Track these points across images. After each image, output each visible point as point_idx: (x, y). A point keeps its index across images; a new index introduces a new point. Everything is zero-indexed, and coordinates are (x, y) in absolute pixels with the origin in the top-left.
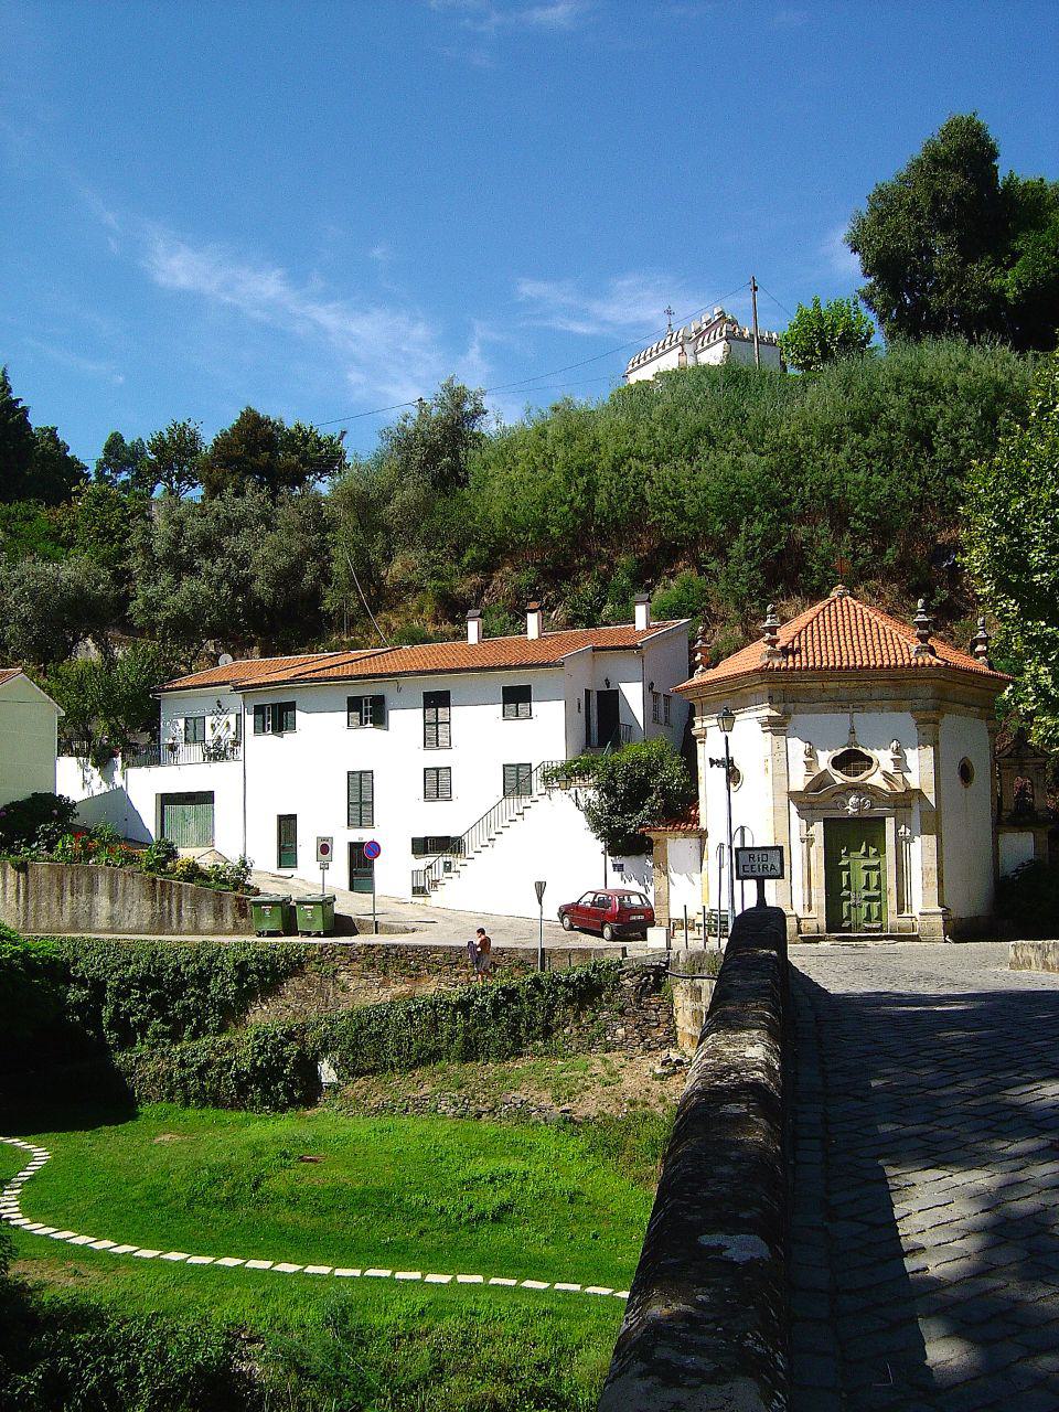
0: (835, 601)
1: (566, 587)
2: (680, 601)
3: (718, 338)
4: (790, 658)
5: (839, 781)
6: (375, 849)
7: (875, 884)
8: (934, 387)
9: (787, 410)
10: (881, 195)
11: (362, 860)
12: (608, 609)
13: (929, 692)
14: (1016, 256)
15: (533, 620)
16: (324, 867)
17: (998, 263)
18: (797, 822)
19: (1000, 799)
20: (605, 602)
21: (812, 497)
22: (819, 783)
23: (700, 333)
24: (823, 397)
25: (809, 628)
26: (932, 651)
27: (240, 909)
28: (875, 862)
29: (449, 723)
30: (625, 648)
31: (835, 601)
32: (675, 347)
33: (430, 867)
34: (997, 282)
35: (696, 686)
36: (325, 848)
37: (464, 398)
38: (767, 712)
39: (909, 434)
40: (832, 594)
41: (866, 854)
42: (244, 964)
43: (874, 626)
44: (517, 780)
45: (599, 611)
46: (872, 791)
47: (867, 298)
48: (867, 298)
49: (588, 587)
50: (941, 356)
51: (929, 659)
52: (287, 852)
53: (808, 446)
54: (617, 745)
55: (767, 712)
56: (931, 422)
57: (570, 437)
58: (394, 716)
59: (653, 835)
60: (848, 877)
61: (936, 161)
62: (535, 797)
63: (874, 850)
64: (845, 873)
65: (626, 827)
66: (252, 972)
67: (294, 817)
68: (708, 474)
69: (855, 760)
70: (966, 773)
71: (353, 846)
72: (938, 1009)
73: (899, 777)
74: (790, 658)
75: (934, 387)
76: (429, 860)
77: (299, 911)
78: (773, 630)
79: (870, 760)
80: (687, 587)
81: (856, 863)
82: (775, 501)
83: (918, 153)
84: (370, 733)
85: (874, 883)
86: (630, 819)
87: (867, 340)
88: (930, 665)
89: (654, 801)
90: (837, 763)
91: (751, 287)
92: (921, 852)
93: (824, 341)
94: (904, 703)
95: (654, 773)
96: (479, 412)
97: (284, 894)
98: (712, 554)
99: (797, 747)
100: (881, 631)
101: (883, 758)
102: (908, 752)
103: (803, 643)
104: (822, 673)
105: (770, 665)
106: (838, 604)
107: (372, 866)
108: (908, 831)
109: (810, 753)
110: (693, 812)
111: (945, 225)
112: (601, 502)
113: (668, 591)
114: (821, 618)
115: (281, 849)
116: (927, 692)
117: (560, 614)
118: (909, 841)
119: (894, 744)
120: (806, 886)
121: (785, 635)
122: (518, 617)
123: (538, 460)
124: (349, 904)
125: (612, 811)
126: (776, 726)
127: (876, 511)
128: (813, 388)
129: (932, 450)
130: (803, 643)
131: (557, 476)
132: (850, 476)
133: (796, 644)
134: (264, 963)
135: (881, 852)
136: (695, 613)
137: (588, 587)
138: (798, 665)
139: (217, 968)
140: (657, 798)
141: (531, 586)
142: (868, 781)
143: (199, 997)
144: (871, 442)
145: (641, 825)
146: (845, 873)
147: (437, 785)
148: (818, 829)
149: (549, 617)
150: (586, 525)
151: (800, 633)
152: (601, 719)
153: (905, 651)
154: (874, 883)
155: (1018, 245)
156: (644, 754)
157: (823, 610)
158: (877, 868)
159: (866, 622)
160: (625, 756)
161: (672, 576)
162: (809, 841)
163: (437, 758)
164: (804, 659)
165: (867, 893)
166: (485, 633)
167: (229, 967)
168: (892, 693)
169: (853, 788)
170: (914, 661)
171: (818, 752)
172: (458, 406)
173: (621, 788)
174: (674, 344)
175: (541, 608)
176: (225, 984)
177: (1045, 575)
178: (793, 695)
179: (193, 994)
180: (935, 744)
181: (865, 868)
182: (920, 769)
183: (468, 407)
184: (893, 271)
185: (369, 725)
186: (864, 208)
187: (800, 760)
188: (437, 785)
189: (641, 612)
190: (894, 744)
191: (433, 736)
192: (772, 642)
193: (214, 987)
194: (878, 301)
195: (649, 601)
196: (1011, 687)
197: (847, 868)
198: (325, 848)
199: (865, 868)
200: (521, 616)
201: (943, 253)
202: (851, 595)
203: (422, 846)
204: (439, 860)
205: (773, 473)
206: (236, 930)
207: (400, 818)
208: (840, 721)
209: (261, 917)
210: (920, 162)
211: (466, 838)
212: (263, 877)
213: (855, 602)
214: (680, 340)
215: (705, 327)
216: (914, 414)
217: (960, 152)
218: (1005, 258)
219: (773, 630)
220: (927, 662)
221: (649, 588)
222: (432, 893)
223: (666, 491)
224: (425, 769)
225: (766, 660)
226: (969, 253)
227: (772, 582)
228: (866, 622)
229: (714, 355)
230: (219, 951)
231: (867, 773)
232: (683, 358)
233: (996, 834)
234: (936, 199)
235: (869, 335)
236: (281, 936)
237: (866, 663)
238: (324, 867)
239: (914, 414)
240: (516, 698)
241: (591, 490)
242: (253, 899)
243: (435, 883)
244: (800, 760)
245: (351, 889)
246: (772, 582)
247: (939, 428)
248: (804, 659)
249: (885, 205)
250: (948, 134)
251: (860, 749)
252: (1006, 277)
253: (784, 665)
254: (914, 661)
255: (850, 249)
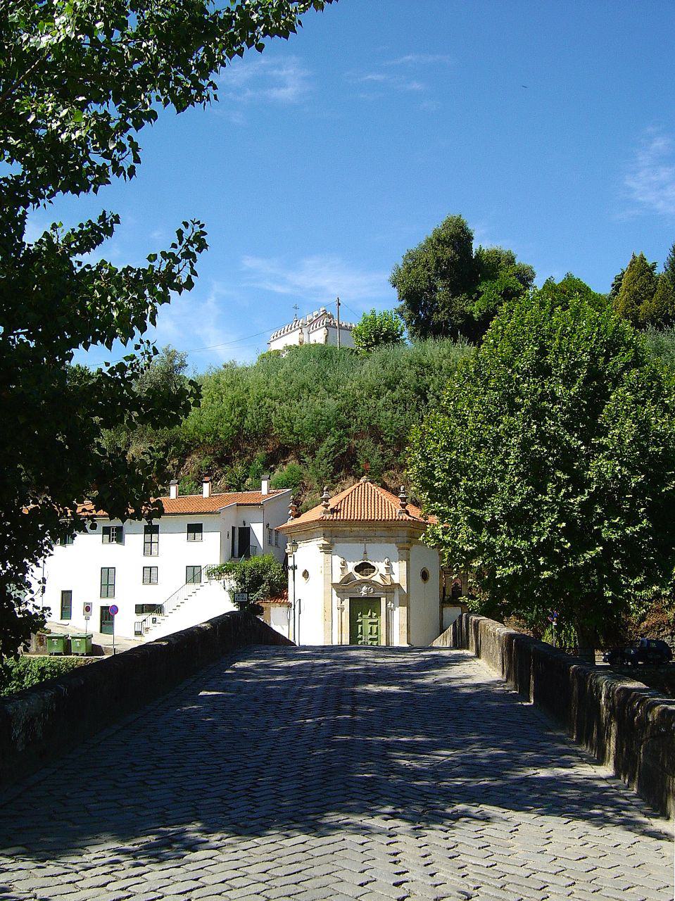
0: (362, 484)
1: (227, 468)
2: (288, 479)
3: (321, 326)
4: (335, 514)
5: (358, 578)
6: (115, 609)
7: (375, 632)
8: (429, 366)
9: (351, 375)
10: (410, 256)
11: (108, 615)
12: (249, 481)
13: (405, 534)
14: (480, 294)
15: (206, 487)
16: (87, 619)
17: (470, 298)
18: (336, 599)
19: (444, 589)
20: (248, 477)
21: (362, 424)
22: (348, 579)
23: (312, 322)
24: (371, 369)
25: (347, 499)
26: (407, 513)
27: (40, 641)
28: (375, 621)
29: (145, 543)
30: (254, 505)
31: (362, 484)
32: (298, 329)
33: (145, 620)
34: (469, 308)
35: (289, 527)
36: (88, 609)
37: (174, 357)
38: (323, 542)
39: (415, 391)
40: (361, 480)
41: (371, 616)
42: (44, 668)
43: (380, 498)
44: (193, 574)
45: (244, 482)
46: (374, 584)
47: (400, 313)
48: (400, 313)
49: (239, 469)
50: (435, 349)
51: (405, 516)
52: (66, 612)
53: (361, 396)
54: (248, 556)
55: (323, 542)
56: (427, 385)
57: (231, 385)
58: (127, 537)
59: (263, 605)
60: (362, 628)
61: (439, 241)
62: (202, 583)
63: (375, 614)
64: (360, 626)
65: (249, 600)
66: (47, 672)
67: (71, 592)
68: (304, 412)
69: (367, 568)
70: (425, 576)
71: (103, 608)
72: (543, 773)
73: (388, 577)
74: (335, 514)
75: (429, 366)
76: (144, 616)
77: (73, 642)
78: (327, 500)
79: (374, 568)
80: (292, 471)
81: (365, 621)
82: (343, 426)
83: (430, 235)
84: (115, 546)
85: (375, 631)
86: (252, 596)
87: (401, 334)
88: (405, 520)
89: (265, 587)
90: (358, 569)
91: (337, 303)
92: (399, 615)
93: (381, 336)
94: (391, 539)
95: (265, 572)
96: (183, 365)
97: (65, 633)
98: (306, 453)
99: (337, 560)
100: (383, 501)
101: (381, 567)
102: (393, 564)
103: (342, 507)
104: (350, 522)
105: (324, 518)
106: (363, 486)
107: (113, 619)
108: (392, 605)
109: (344, 564)
110: (285, 593)
111: (443, 276)
112: (247, 423)
113: (281, 473)
114: (353, 493)
115: (62, 609)
116: (404, 533)
117: (222, 483)
118: (393, 610)
119: (386, 560)
120: (340, 632)
121: (333, 503)
122: (199, 484)
123: (215, 396)
124: (100, 640)
125: (243, 591)
126: (327, 549)
127: (397, 433)
128: (367, 364)
129: (426, 401)
130: (342, 507)
131: (225, 407)
132: (383, 413)
133: (339, 507)
134: (54, 668)
135: (378, 615)
136: (296, 485)
137: (239, 469)
138: (338, 518)
139: (28, 670)
140: (266, 585)
141: (206, 467)
142: (372, 579)
143: (18, 686)
144: (396, 395)
145: (258, 600)
146: (360, 626)
147: (150, 575)
148: (346, 602)
149: (216, 485)
150: (240, 433)
151: (341, 501)
152: (241, 542)
153: (394, 512)
154: (375, 631)
155: (480, 288)
156: (261, 562)
157: (355, 489)
158: (376, 623)
159: (376, 496)
160: (250, 563)
161: (285, 463)
162: (342, 609)
163: (150, 561)
164: (342, 515)
165: (370, 637)
166: (181, 493)
167: (35, 670)
168: (386, 534)
169: (365, 582)
170: (398, 518)
171: (348, 563)
172: (171, 361)
173: (248, 580)
174: (297, 327)
175: (211, 481)
176: (33, 679)
177: (440, 483)
178: (335, 533)
179: (15, 684)
180: (408, 560)
181: (370, 623)
182: (399, 573)
183: (177, 362)
184: (415, 299)
185: (115, 542)
186: (400, 262)
187: (337, 567)
188: (150, 575)
189: (264, 484)
190: (386, 560)
191: (148, 549)
192: (326, 506)
193: (27, 680)
194: (406, 314)
195: (269, 478)
196: (424, 535)
197: (361, 623)
198: (88, 609)
199: (370, 623)
200: (200, 484)
201: (442, 293)
202: (370, 481)
203: (141, 609)
204: (148, 617)
205: (341, 409)
206: (38, 652)
207: (128, 594)
208: (359, 547)
209: (52, 645)
210: (431, 241)
211: (164, 605)
212: (52, 624)
213: (372, 485)
214: (300, 325)
215: (315, 318)
216: (418, 381)
217: (452, 236)
218: (474, 295)
219: (327, 500)
220: (404, 518)
221: (272, 470)
222: (145, 634)
223: (283, 418)
224: (144, 567)
225: (323, 515)
226: (455, 290)
227: (337, 470)
228: (376, 496)
229: (318, 337)
230: (30, 661)
231: (372, 574)
232: (302, 336)
233: (442, 608)
234: (438, 261)
235: (402, 332)
236: (62, 655)
237: (373, 518)
238: (87, 619)
239: (418, 381)
240: (195, 529)
241: (243, 414)
242: (47, 635)
243: (147, 629)
244: (337, 567)
245: (101, 632)
246: (337, 470)
247: (431, 389)
248: (342, 515)
249: (413, 260)
250: (446, 227)
251: (369, 562)
252: (474, 305)
253: (331, 518)
254: (398, 518)
255: (391, 285)
